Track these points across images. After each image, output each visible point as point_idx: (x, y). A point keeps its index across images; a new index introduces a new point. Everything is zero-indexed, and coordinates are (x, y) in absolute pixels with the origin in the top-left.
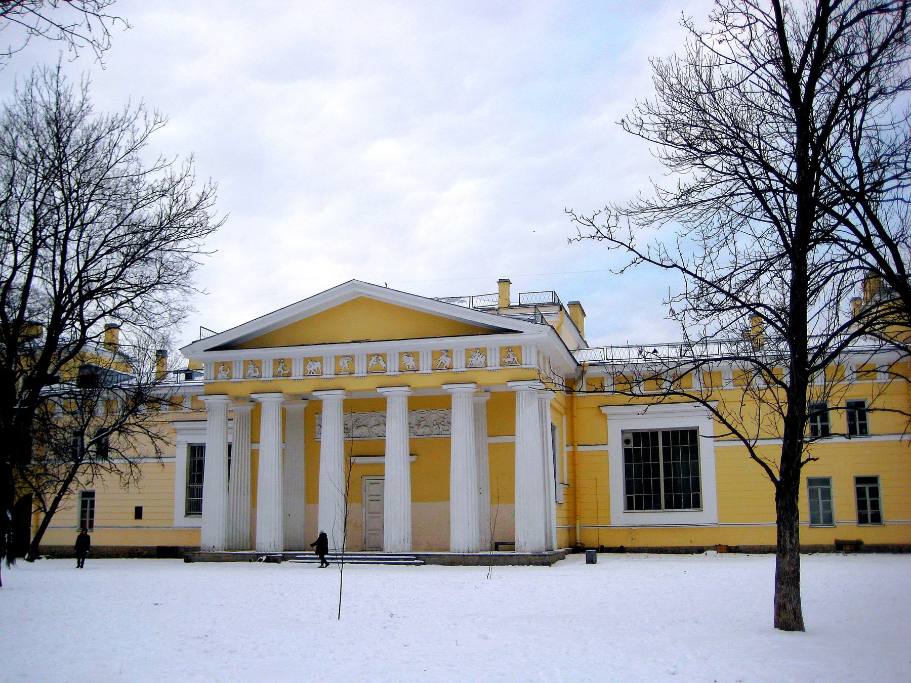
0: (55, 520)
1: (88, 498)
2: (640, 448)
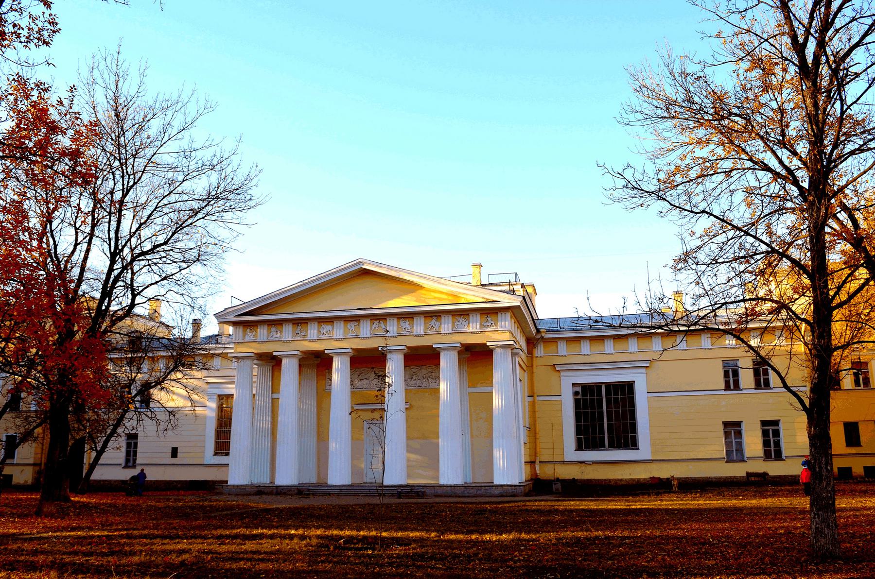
0: (105, 458)
1: (132, 438)
2: (588, 398)
